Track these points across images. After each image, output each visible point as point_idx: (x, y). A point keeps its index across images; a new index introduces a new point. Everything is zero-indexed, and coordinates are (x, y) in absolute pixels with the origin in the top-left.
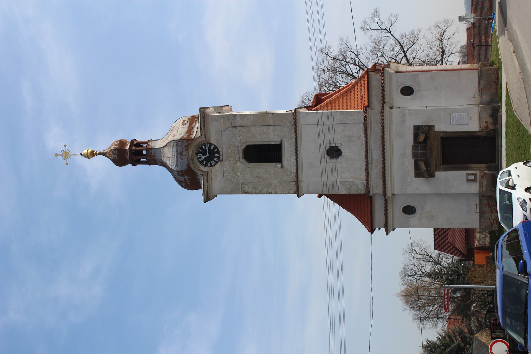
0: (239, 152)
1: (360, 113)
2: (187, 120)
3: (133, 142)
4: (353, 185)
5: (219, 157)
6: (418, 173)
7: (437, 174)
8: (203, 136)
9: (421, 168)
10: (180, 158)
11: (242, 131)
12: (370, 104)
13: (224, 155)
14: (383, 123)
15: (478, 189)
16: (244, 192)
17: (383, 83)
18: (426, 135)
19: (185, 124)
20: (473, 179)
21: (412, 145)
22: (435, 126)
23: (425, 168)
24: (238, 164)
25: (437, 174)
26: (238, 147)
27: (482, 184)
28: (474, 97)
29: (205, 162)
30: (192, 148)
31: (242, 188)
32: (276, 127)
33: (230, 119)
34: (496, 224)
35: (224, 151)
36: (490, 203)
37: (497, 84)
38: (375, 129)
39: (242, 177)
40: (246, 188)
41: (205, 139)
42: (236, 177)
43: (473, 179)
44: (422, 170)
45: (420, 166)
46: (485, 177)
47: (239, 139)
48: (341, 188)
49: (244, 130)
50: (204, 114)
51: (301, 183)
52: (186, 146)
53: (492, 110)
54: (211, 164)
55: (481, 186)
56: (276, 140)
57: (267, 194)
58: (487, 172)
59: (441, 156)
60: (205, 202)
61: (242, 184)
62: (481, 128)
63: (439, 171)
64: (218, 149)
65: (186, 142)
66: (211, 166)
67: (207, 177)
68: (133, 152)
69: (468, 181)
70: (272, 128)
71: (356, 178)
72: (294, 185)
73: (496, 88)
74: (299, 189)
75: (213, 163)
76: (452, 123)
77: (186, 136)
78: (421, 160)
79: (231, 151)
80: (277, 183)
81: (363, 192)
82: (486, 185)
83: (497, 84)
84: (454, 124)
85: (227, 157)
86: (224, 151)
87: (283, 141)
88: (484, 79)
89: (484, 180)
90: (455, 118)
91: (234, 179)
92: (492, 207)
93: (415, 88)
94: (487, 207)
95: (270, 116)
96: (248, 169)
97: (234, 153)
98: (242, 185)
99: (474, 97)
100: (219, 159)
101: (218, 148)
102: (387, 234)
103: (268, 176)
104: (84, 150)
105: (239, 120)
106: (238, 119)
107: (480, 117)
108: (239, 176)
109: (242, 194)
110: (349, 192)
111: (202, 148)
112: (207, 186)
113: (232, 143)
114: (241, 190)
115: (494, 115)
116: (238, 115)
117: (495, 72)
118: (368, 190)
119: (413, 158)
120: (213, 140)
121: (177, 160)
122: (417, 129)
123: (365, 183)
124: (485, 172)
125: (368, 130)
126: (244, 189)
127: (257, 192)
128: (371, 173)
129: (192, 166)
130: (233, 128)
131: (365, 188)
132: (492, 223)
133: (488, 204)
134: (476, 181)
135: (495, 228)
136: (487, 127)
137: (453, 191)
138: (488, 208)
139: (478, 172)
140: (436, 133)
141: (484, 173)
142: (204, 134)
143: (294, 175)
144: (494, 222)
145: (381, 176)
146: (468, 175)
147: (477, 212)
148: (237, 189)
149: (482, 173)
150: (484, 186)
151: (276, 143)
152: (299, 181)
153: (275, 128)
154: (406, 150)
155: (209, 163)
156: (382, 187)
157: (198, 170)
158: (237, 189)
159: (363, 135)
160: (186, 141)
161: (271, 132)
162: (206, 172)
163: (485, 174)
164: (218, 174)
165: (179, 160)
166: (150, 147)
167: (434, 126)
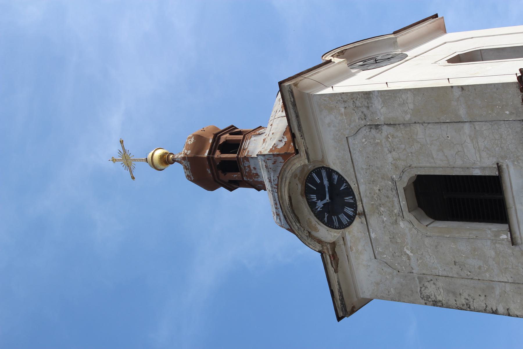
3: (219, 138)
5: (354, 206)
11: (393, 136)
13: (365, 200)
24: (402, 224)
26: (392, 180)
30: (287, 183)
31: (421, 288)
32: (477, 126)
40: (431, 290)
42: (404, 258)
47: (390, 158)
49: (399, 134)
50: (293, 96)
57: (485, 311)
60: (339, 319)
61: (420, 279)
64: (349, 185)
66: (342, 226)
75: (344, 219)
77: (281, 145)
79: (379, 190)
80: (507, 285)
85: (373, 204)
86: (362, 188)
87: (504, 167)
91: (398, 264)
95: (457, 93)
96: (427, 241)
97: (388, 197)
98: (420, 282)
100: (356, 210)
101: (347, 182)
105: (380, 107)
106: (377, 104)
108: (409, 258)
109: (426, 304)
111: (314, 183)
112: (336, 280)
114: (421, 294)
126: (427, 292)
127: (459, 304)
129: (297, 228)
130: (371, 128)
151: (487, 173)
155: (334, 218)
158: (412, 291)
160: (280, 159)
161: (468, 140)
162: (329, 246)
164: (360, 248)
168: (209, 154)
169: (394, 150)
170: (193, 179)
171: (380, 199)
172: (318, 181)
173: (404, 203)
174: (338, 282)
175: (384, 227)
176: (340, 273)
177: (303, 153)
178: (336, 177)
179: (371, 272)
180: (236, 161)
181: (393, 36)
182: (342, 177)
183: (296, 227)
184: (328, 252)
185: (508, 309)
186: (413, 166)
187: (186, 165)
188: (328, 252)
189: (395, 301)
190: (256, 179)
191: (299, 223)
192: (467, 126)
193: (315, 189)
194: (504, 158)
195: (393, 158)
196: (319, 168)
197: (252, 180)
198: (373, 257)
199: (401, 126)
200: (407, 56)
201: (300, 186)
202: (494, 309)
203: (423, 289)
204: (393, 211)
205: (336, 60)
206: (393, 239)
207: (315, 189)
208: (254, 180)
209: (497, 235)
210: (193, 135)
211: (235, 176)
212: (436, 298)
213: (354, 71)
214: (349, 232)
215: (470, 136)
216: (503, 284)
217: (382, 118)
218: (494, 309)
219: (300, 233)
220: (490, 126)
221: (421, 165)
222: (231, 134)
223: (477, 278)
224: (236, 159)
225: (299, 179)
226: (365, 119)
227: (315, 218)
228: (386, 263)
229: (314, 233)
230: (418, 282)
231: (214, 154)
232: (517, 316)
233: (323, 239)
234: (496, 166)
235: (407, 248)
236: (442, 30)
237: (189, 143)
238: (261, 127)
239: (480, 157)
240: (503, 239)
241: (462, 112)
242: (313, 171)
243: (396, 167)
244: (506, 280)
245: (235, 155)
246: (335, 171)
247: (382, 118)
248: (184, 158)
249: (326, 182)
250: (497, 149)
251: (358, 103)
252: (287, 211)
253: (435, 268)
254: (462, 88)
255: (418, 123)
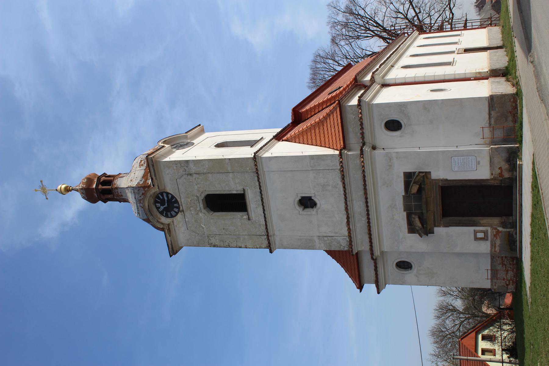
0: (199, 202)
1: (334, 157)
2: (144, 160)
3: (100, 179)
4: (333, 241)
5: (178, 208)
6: (412, 229)
7: (436, 229)
8: (156, 187)
9: (415, 225)
10: (140, 206)
11: (198, 178)
12: (346, 145)
13: (183, 205)
14: (364, 171)
15: (489, 248)
16: (211, 245)
17: (361, 118)
18: (420, 185)
19: (142, 165)
20: (483, 237)
21: (403, 196)
22: (431, 173)
23: (420, 225)
24: (200, 214)
25: (436, 229)
26: (197, 196)
27: (495, 243)
28: (483, 138)
29: (165, 212)
30: (148, 199)
31: (208, 240)
32: (235, 174)
33: (183, 166)
34: (513, 285)
35: (183, 200)
36: (504, 261)
37: (514, 115)
38: (355, 176)
39: (207, 229)
40: (213, 241)
41: (159, 189)
42: (201, 228)
43: (483, 237)
44: (417, 228)
45: (414, 223)
46: (499, 235)
47: (196, 187)
48: (320, 244)
49: (201, 177)
50: (153, 162)
51: (273, 238)
52: (143, 194)
53: (508, 152)
54: (171, 214)
55: (493, 245)
56: (238, 189)
57: (236, 247)
58: (500, 229)
59: (441, 208)
60: (171, 256)
61: (208, 237)
62: (493, 175)
63: (439, 226)
64: (176, 199)
65: (143, 189)
66: (172, 216)
67: (169, 230)
68: (101, 191)
69: (476, 239)
70: (231, 175)
71: (337, 233)
72: (265, 239)
73: (515, 121)
74: (271, 244)
75: (173, 213)
76: (454, 169)
77: (141, 183)
78: (415, 214)
79: (191, 201)
80: (246, 236)
81: (346, 249)
82: (500, 244)
83: (514, 115)
84: (456, 169)
85: (187, 207)
86: (183, 200)
87: (246, 190)
88: (497, 109)
89: (497, 238)
90: (458, 163)
91: (198, 231)
92: (507, 265)
93: (403, 121)
94: (501, 265)
95: (227, 161)
96: (212, 221)
97: (194, 203)
98: (208, 238)
99: (483, 138)
100: (179, 209)
101: (175, 198)
102: (379, 293)
103: (235, 229)
104: (58, 186)
105: (193, 167)
106: (191, 165)
107: (492, 162)
108: (203, 228)
109: (210, 247)
110: (329, 249)
111: (159, 198)
112: (170, 240)
113: (190, 191)
114: (208, 243)
115: (511, 159)
116: (191, 161)
117: (512, 100)
118: (351, 248)
119: (404, 211)
120: (170, 189)
121: (138, 208)
122: (409, 177)
123: (348, 240)
124: (498, 230)
125: (345, 179)
126: (211, 242)
127: (225, 245)
128: (354, 228)
129: (151, 219)
130: (188, 175)
131: (348, 244)
132: (508, 283)
133: (502, 263)
134: (487, 240)
135: (510, 289)
136: (501, 175)
137: (458, 250)
138: (502, 266)
139: (489, 229)
140: (434, 181)
141: (497, 230)
142: (157, 184)
143: (264, 228)
144: (509, 282)
145: (367, 231)
146: (475, 232)
147: (488, 279)
148: (204, 242)
149: (495, 231)
150: (497, 245)
151: (239, 192)
152: (270, 236)
153: (235, 175)
154: (396, 201)
155: (169, 213)
156: (369, 244)
157: (158, 223)
158: (204, 242)
159: (340, 184)
160: (142, 189)
161: (231, 179)
162: (167, 225)
163: (498, 232)
164: (180, 225)
165: (140, 209)
166: (116, 186)
167: (430, 172)
168: (96, 186)
169: (198, 184)
170: (86, 198)
171: (191, 205)
172: (161, 198)
173: (202, 206)
174: (171, 240)
175: (192, 216)
176: (171, 236)
177: (156, 187)
178: (170, 196)
179: (186, 235)
180: (111, 190)
181: (185, 134)
182: (173, 196)
183: (151, 218)
184: (167, 228)
185: (246, 246)
186: (207, 190)
187: (83, 192)
188: (167, 228)
189: (196, 246)
190: (121, 198)
191: (153, 216)
192: (231, 174)
193: (160, 201)
194: (246, 186)
195: (197, 187)
196: (162, 192)
197: (119, 198)
198: (187, 229)
199: (202, 174)
200: (194, 143)
201: (152, 200)
202: (240, 246)
203: (209, 241)
204: (196, 209)
205: (167, 146)
206: (196, 221)
207: (160, 201)
208: (120, 198)
209: (242, 216)
210: (86, 178)
211: (109, 196)
212: (215, 244)
213: (174, 150)
214: (176, 219)
215: (232, 178)
216: (244, 236)
217: (193, 171)
218: (240, 246)
219: (153, 220)
220: (241, 174)
221: (210, 190)
222: (106, 177)
223: (233, 234)
224: (111, 189)
225: (152, 197)
226: (186, 171)
227: (159, 214)
228: (193, 231)
229: (159, 220)
230: (207, 237)
231: (98, 187)
232: (250, 248)
233: (164, 223)
234: (243, 190)
235: (203, 224)
236: (202, 131)
237: (84, 181)
238: (120, 173)
239: (236, 186)
240: (245, 218)
241: (229, 169)
242: (159, 194)
243: (199, 191)
244: (245, 234)
245: (111, 187)
246: (170, 193)
247: (193, 171)
248: (82, 189)
249: (166, 198)
250: (243, 183)
251: (182, 165)
252: (147, 212)
253: (215, 232)
254: (230, 159)
255: (210, 173)
